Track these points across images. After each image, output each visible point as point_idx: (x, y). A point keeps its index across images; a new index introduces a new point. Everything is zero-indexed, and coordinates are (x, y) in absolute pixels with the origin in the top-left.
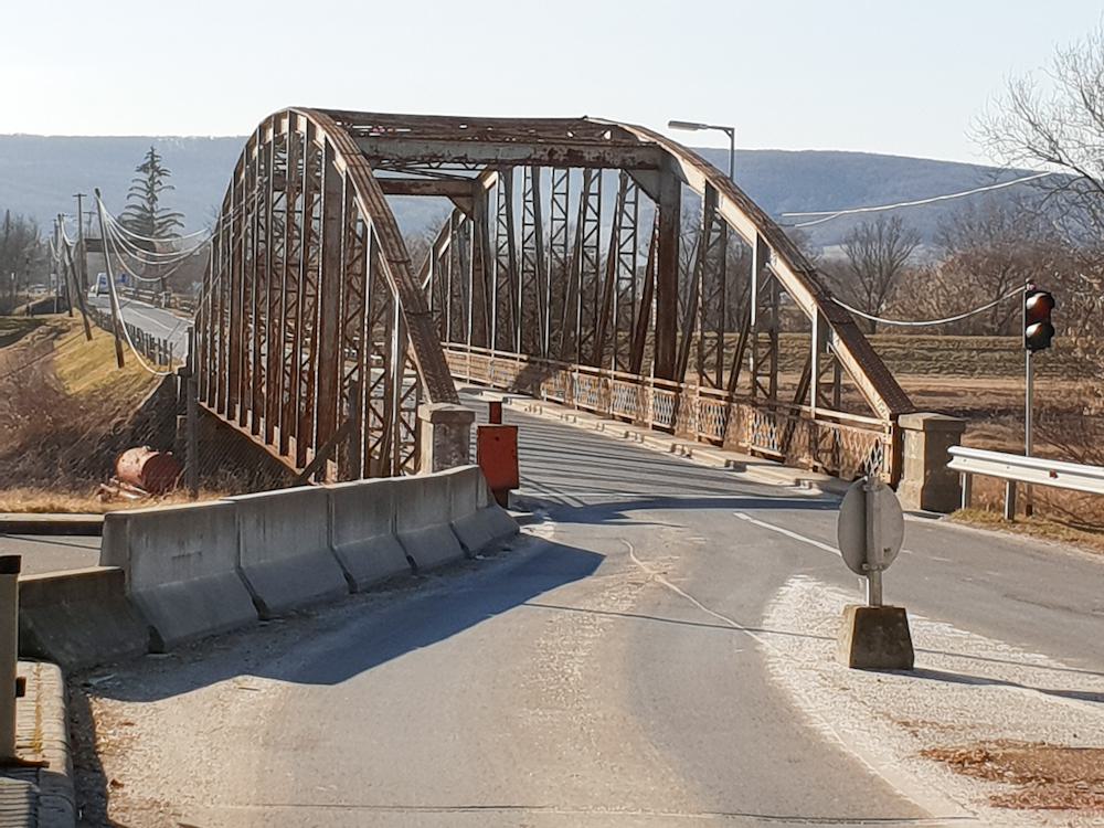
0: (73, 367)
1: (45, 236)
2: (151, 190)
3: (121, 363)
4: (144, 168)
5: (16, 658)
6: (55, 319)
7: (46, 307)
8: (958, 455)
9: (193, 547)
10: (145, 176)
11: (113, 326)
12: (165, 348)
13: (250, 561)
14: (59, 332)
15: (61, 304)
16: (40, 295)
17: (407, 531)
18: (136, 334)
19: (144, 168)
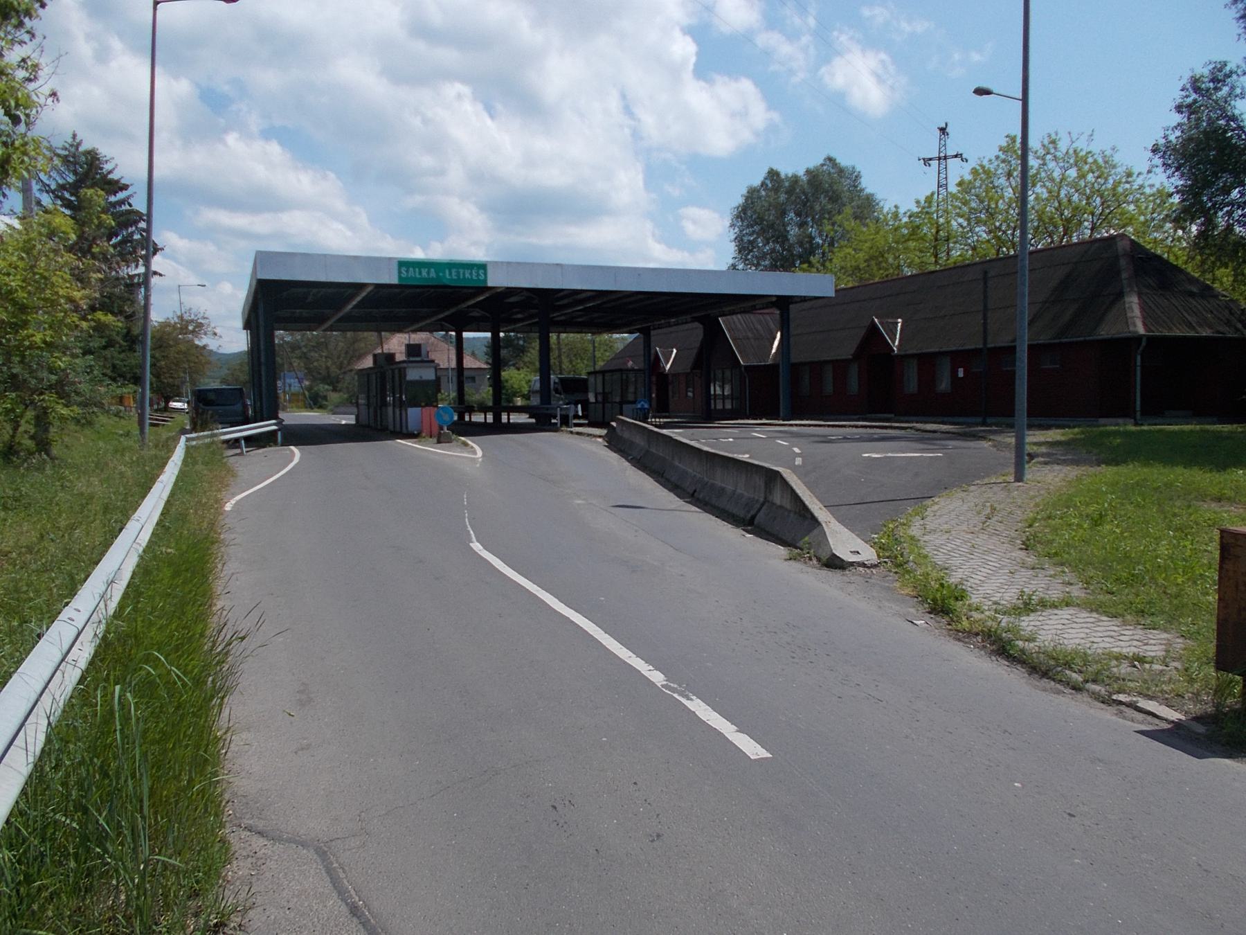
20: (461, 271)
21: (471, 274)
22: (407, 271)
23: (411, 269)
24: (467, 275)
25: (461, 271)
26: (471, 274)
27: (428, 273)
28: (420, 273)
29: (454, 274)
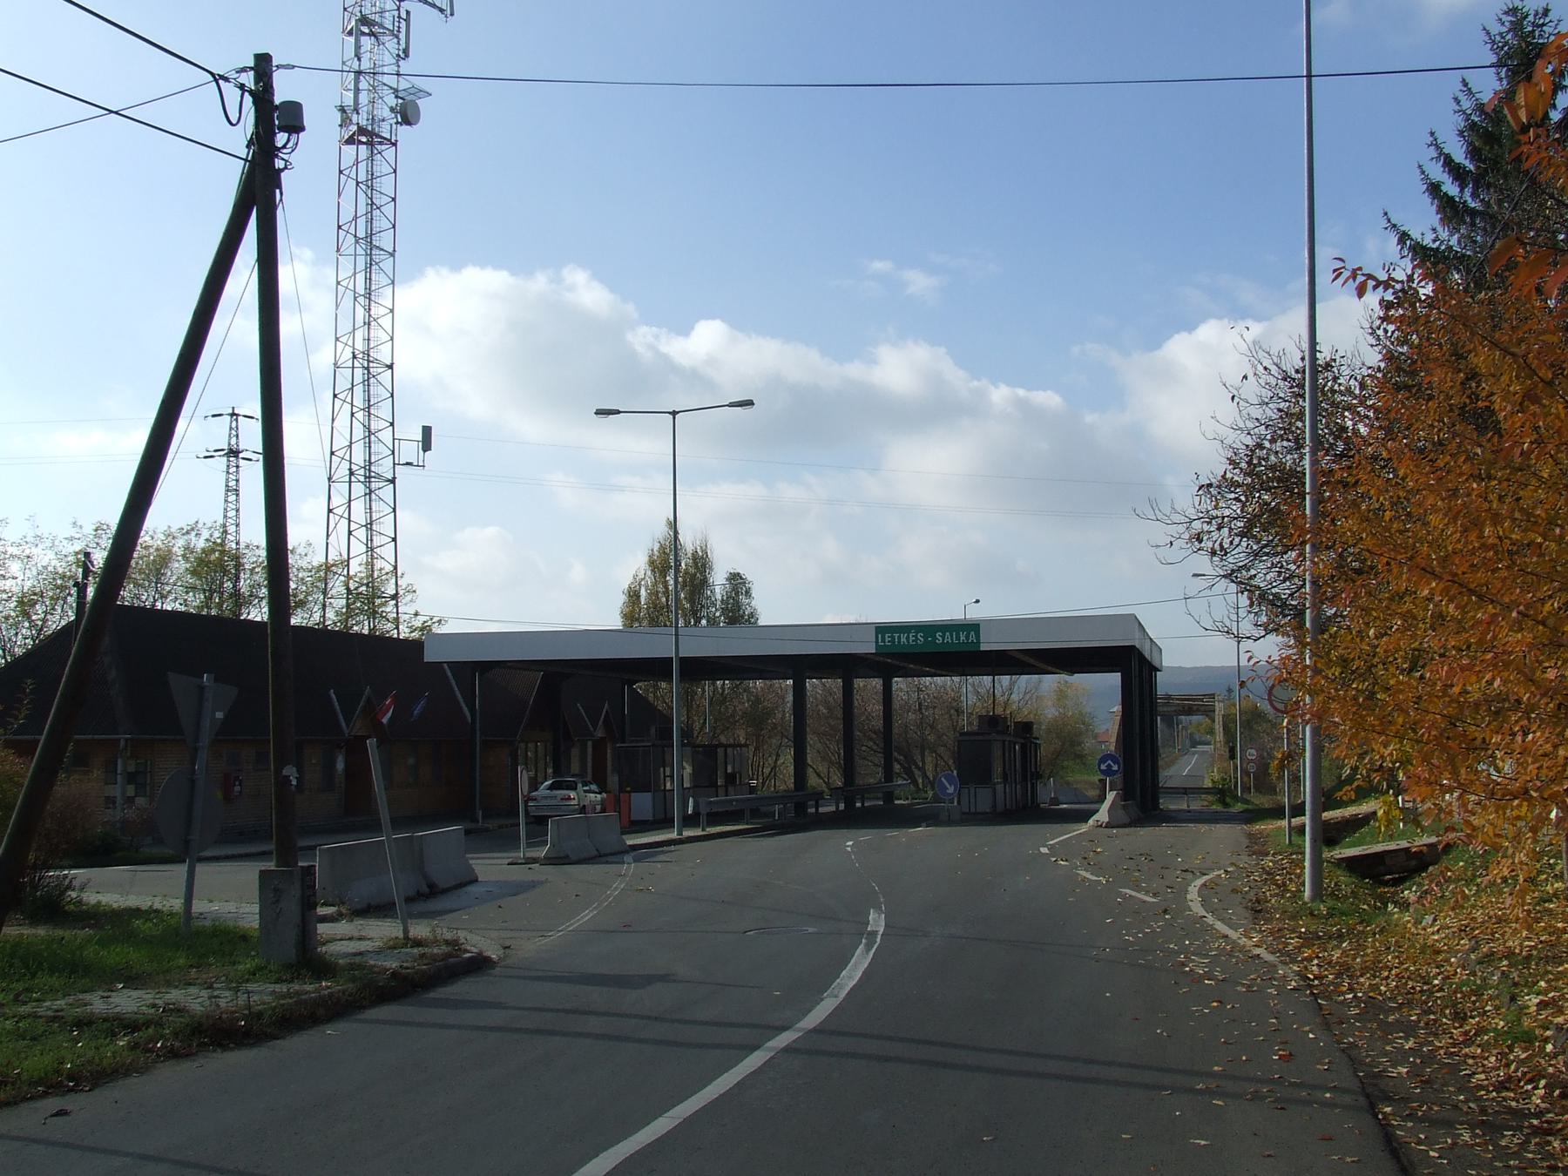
21: (908, 638)
23: (948, 634)
24: (903, 640)
26: (908, 638)
27: (967, 638)
28: (958, 638)
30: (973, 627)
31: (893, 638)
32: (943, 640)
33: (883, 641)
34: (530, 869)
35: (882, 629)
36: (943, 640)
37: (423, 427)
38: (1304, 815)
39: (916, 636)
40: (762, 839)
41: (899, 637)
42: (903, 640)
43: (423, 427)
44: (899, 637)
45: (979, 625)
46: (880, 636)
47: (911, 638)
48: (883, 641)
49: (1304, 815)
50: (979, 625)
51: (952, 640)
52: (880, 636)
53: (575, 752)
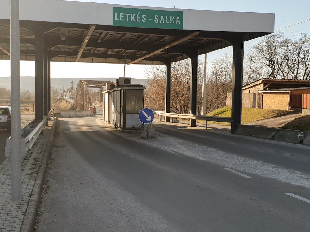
0: (62, 105)
1: (59, 91)
2: (72, 85)
3: (249, 91)
4: (71, 83)
5: (20, 59)
6: (60, 100)
7: (59, 99)
8: (285, 114)
9: (65, 113)
10: (71, 84)
11: (66, 101)
12: (71, 103)
13: (69, 114)
14: (61, 102)
15: (61, 99)
16: (59, 98)
17: (82, 114)
18: (69, 101)
19: (71, 83)
20: (128, 15)
21: (135, 18)
22: (159, 19)
24: (132, 18)
25: (128, 15)
26: (135, 18)
27: (175, 20)
28: (169, 20)
29: (121, 17)
30: (179, 14)
31: (125, 16)
32: (159, 21)
33: (118, 17)
34: (13, 201)
35: (117, 10)
36: (159, 21)
37: (113, 7)
38: (167, 112)
39: (141, 17)
40: (252, 101)
41: (130, 16)
42: (132, 18)
43: (113, 7)
44: (130, 16)
45: (182, 12)
46: (116, 14)
47: (138, 18)
48: (118, 17)
49: (167, 112)
50: (182, 12)
51: (165, 21)
52: (116, 14)
53: (115, 120)
